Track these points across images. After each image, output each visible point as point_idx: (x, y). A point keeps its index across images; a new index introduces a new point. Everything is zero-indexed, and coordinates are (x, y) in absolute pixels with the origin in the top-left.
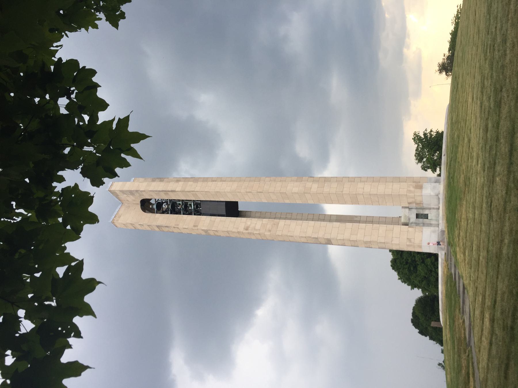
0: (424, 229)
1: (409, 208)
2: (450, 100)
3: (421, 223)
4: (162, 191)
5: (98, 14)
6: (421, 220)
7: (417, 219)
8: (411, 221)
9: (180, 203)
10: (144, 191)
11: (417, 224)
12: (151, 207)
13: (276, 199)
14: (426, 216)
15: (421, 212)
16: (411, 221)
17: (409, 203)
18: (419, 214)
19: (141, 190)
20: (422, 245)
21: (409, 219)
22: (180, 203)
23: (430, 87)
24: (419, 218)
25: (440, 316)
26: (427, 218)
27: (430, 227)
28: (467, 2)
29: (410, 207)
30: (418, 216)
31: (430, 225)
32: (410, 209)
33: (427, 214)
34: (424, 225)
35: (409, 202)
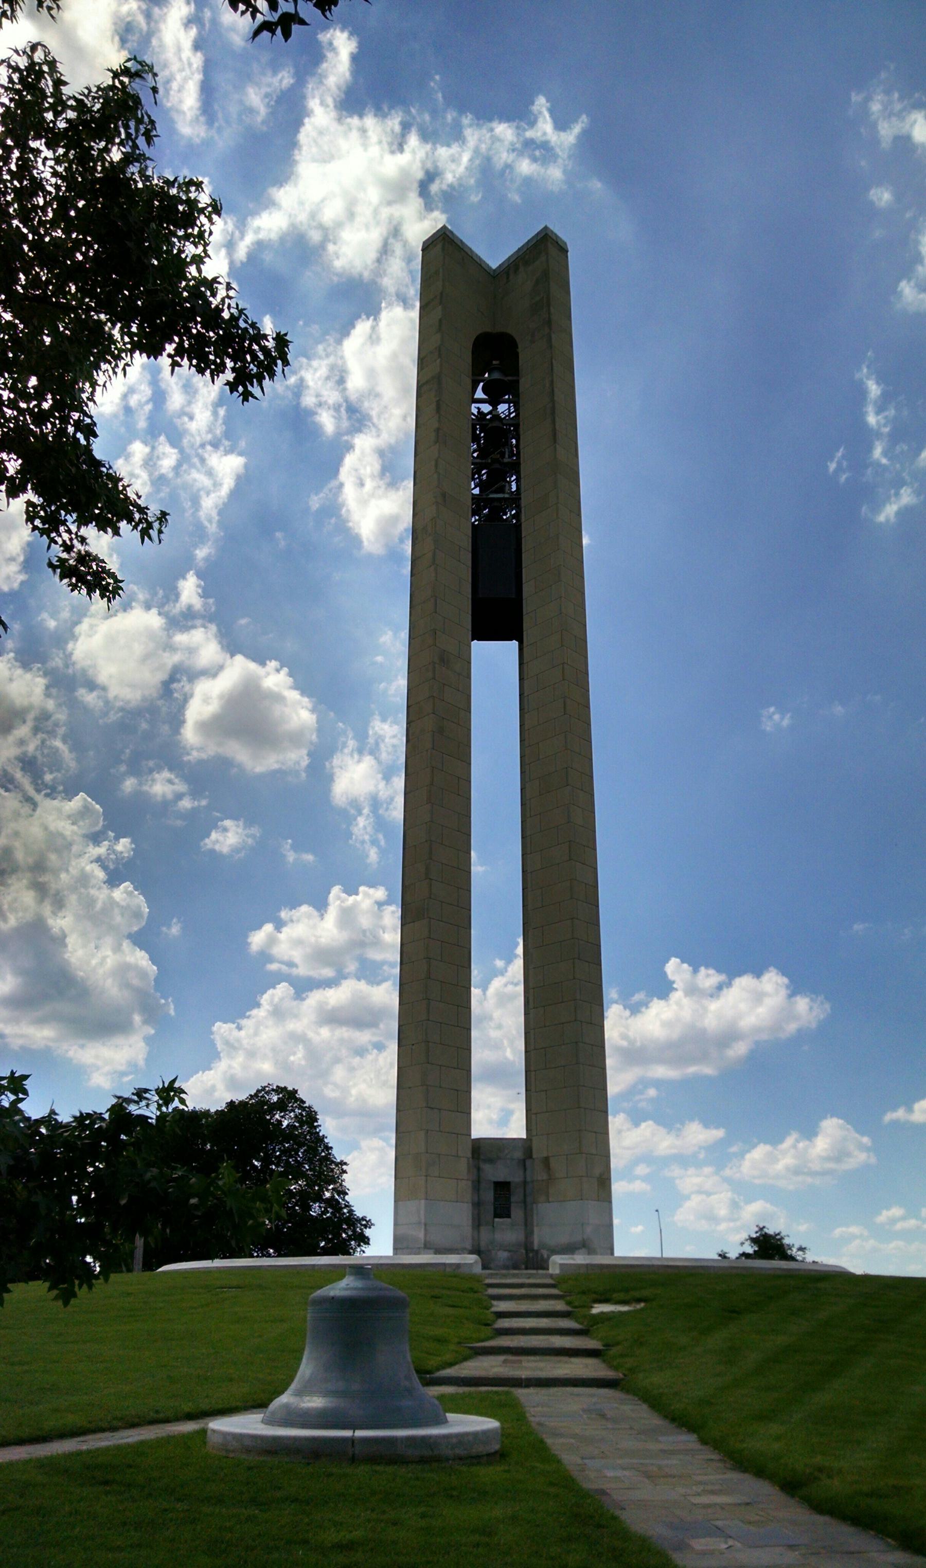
0: (465, 1205)
1: (524, 1161)
2: (826, 1271)
3: (479, 1199)
4: (553, 401)
5: (11, 319)
6: (489, 1196)
7: (492, 1186)
8: (487, 1168)
9: (507, 456)
10: (550, 346)
11: (477, 1185)
12: (494, 362)
13: (541, 757)
14: (502, 1211)
15: (516, 1197)
16: (487, 1168)
17: (546, 1161)
18: (509, 1190)
19: (553, 336)
20: (540, 1205)
21: (491, 1161)
22: (507, 456)
23: (657, 1211)
24: (495, 1190)
25: (184, 1263)
26: (497, 1215)
27: (470, 1223)
28: (560, 1306)
29: (528, 1163)
30: (502, 1188)
31: (477, 1223)
32: (523, 1164)
33: (509, 1216)
34: (477, 1205)
35: (552, 1161)
